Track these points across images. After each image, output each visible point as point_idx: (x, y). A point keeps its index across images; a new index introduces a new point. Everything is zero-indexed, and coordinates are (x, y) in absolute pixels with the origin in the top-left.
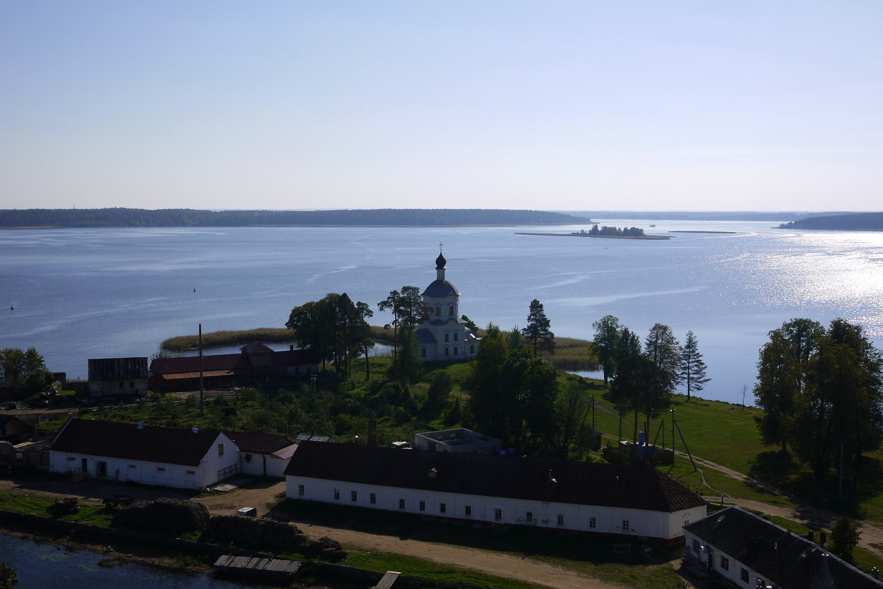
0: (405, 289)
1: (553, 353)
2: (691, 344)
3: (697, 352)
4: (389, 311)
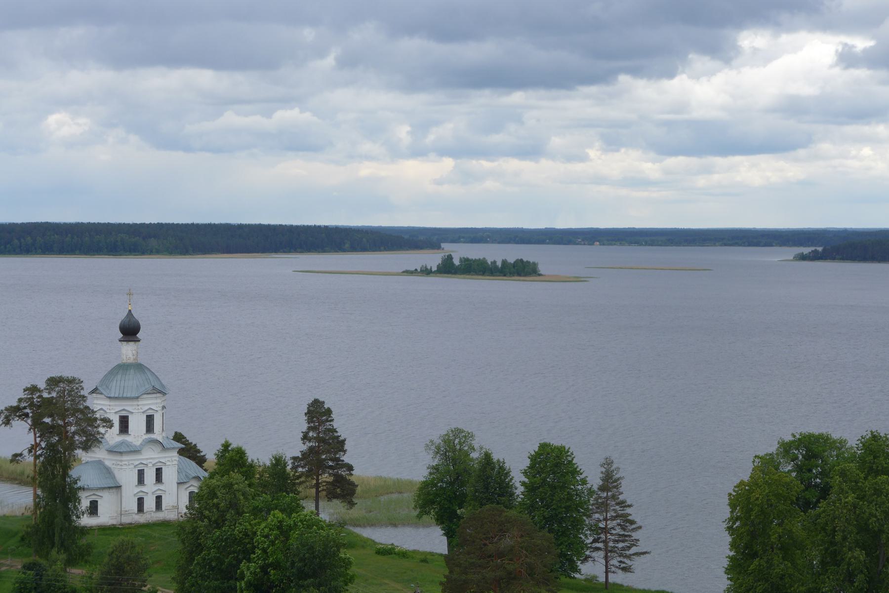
0: (53, 382)
1: (352, 504)
2: (610, 481)
3: (621, 497)
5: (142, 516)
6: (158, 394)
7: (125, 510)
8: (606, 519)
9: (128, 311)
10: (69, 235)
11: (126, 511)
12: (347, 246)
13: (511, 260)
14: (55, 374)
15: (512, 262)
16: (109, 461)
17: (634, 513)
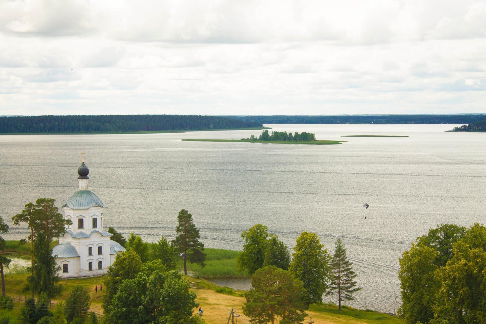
0: (40, 201)
1: (203, 265)
2: (340, 252)
5: (91, 272)
6: (99, 207)
7: (82, 269)
8: (339, 272)
9: (82, 163)
12: (212, 126)
13: (300, 133)
14: (42, 197)
16: (74, 243)
17: (353, 268)
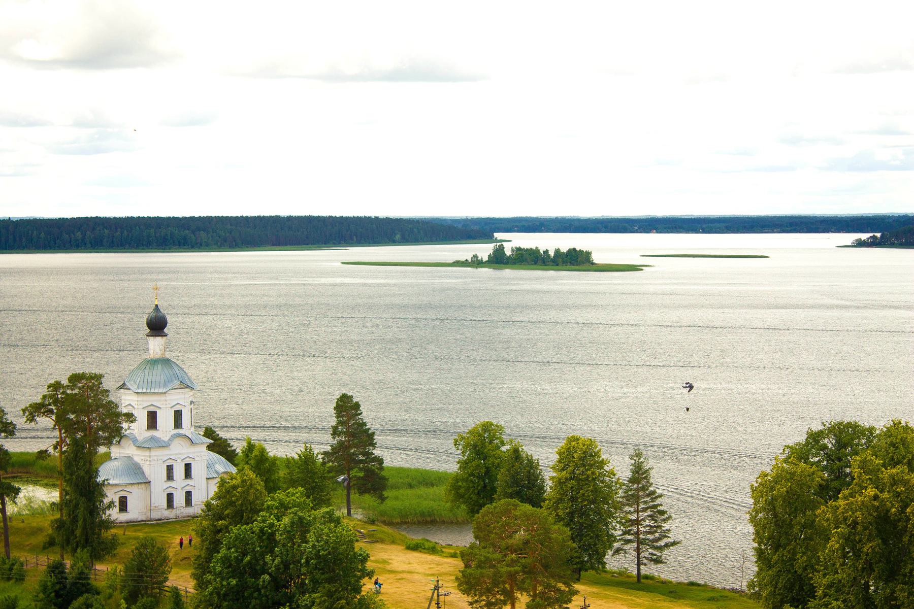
0: (75, 378)
1: (382, 499)
2: (640, 474)
4: (46, 421)
5: (172, 512)
7: (154, 505)
8: (637, 511)
9: (154, 306)
10: (119, 230)
11: (156, 507)
12: (398, 237)
13: (564, 250)
15: (565, 251)
17: (665, 503)
